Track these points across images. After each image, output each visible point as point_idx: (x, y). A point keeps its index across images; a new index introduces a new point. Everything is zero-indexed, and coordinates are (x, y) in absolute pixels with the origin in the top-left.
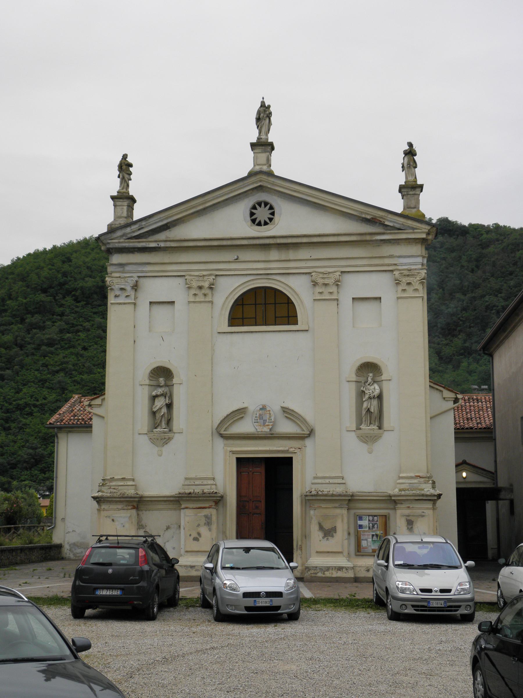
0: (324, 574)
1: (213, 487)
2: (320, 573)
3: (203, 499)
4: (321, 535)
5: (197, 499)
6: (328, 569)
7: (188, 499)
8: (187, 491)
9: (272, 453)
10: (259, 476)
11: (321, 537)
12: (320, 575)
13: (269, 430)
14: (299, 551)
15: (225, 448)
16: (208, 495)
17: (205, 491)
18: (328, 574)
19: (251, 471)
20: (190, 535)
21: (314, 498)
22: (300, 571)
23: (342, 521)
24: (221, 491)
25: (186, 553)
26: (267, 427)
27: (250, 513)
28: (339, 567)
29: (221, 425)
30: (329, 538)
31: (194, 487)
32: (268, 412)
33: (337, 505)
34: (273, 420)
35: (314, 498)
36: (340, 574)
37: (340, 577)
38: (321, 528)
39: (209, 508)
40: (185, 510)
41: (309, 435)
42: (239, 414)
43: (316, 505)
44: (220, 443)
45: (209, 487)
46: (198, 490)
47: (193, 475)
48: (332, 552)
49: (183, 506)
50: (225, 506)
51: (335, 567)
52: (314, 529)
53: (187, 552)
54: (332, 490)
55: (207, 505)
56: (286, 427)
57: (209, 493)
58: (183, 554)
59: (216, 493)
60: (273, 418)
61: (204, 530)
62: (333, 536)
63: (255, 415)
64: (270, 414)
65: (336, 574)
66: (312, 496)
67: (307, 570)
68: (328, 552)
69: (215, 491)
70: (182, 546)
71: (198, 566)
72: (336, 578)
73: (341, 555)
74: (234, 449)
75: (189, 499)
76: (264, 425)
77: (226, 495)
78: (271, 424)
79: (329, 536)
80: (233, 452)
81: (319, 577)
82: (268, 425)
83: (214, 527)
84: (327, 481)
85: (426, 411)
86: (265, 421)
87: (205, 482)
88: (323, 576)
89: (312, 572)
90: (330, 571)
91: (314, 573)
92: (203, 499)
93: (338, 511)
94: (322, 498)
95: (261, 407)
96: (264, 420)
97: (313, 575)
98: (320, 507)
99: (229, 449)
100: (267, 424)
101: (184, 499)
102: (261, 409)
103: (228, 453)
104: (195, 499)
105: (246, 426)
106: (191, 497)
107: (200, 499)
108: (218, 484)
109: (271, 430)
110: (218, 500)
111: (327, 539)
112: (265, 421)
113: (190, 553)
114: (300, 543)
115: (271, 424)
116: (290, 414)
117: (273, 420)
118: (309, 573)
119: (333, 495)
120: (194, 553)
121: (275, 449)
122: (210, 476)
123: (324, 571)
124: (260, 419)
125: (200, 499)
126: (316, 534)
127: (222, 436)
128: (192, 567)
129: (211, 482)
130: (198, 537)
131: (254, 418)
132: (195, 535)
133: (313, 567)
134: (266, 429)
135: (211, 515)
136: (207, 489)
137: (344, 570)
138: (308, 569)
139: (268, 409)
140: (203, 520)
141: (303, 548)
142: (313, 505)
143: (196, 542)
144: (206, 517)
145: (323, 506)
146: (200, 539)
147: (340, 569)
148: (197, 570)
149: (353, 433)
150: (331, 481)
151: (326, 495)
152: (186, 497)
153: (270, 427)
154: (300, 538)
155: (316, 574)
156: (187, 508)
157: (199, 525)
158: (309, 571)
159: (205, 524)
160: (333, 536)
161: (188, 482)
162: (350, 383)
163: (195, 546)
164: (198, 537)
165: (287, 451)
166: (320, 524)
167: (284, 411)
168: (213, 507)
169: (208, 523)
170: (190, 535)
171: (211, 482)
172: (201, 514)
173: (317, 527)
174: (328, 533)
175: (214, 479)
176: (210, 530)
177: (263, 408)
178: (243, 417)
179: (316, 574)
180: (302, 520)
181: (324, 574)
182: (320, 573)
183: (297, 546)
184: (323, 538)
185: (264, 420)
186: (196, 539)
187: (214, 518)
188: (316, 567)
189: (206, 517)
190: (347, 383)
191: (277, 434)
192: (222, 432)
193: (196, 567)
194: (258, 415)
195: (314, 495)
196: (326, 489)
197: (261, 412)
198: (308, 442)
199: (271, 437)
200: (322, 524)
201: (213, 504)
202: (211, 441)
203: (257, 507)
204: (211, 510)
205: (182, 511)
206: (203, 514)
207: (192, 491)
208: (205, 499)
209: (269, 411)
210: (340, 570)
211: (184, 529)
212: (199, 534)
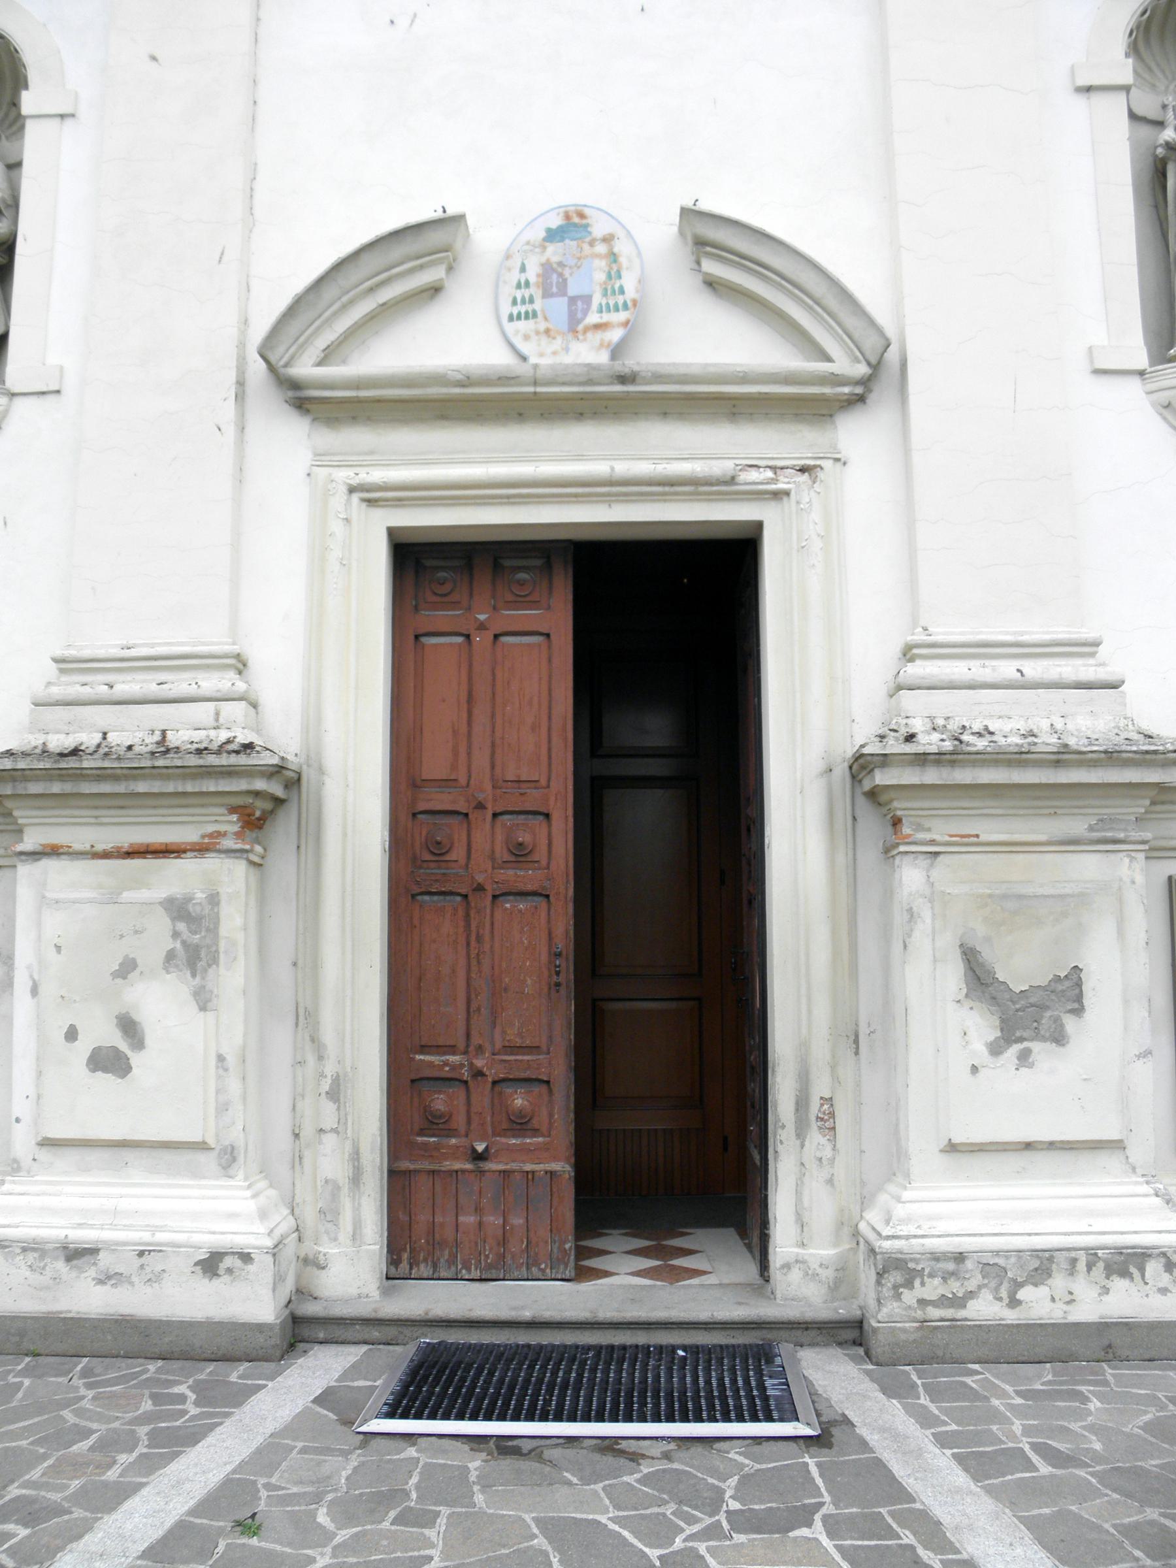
0: (1014, 1303)
1: (235, 711)
2: (986, 1296)
3: (156, 787)
4: (980, 1026)
5: (120, 788)
6: (1042, 1265)
7: (56, 788)
8: (58, 742)
9: (626, 498)
10: (535, 650)
11: (979, 1047)
12: (985, 1309)
13: (603, 358)
14: (816, 1138)
15: (322, 473)
16: (194, 761)
17: (178, 738)
18: (1040, 1304)
19: (482, 627)
20: (72, 1034)
21: (931, 776)
22: (828, 1274)
23: (1121, 933)
24: (283, 738)
25: (44, 1155)
26: (596, 337)
27: (480, 888)
28: (1119, 1250)
29: (295, 327)
30: (1036, 1046)
31: (103, 716)
32: (601, 248)
33: (1077, 826)
34: (631, 293)
35: (931, 776)
36: (1125, 1301)
37: (1127, 1327)
38: (979, 979)
39: (201, 849)
40: (46, 863)
41: (857, 397)
42: (413, 258)
43: (940, 830)
44: (288, 443)
45: (203, 713)
46: (131, 731)
47: (106, 644)
48: (1052, 1146)
49: (30, 841)
50: (310, 838)
51: (1092, 1255)
52: (929, 987)
53: (48, 1143)
54: (1045, 724)
55: (188, 834)
56: (706, 340)
57: (199, 752)
58: (26, 1162)
59: (248, 747)
60: (629, 282)
61: (160, 1001)
62: (1059, 1038)
63: (515, 276)
64: (613, 257)
65: (1094, 1302)
66: (922, 759)
67: (894, 1277)
68: (1028, 1146)
69: (243, 737)
70: (21, 1107)
71: (114, 1247)
72: (1103, 1327)
73: (1112, 1161)
74: (377, 476)
75: (68, 787)
76: (574, 327)
77: (321, 771)
78: (623, 316)
79: (1037, 1036)
80: (372, 496)
81: (983, 1330)
82: (598, 327)
83: (233, 978)
84: (1007, 669)
85: (297, 929)
86: (578, 304)
87: (181, 684)
88: (1011, 1316)
89: (932, 1289)
90: (1059, 1282)
91: (943, 1301)
92: (156, 787)
93: (1088, 867)
94: (987, 776)
95: (556, 221)
96: (573, 300)
97: (934, 1313)
98: (970, 842)
99: (345, 476)
100: (593, 318)
101: (35, 788)
102: (552, 235)
103: (339, 500)
104: (105, 788)
105: (457, 339)
106: (80, 775)
107: (141, 787)
108: (268, 698)
109: (616, 352)
110: (263, 801)
111: (1024, 1058)
112: (578, 304)
113: (72, 1156)
114: (821, 1087)
115: (623, 316)
116: (741, 260)
117: (631, 293)
118: (909, 1297)
119: (1063, 757)
120: (93, 1156)
121: (643, 468)
122: (216, 640)
123: (1017, 1285)
124: (547, 294)
125: (141, 787)
126: (942, 1026)
127: (302, 399)
128: (76, 1254)
129: (223, 682)
130: (123, 1046)
131: (508, 292)
132: (101, 1032)
133: (936, 1257)
134: (588, 354)
135: (214, 899)
136: (188, 727)
137: (1153, 1268)
138: (898, 1269)
139: (598, 230)
140: (160, 933)
141: (842, 1122)
142: (919, 828)
143: (106, 1080)
144: (178, 909)
145: (991, 831)
146: (135, 1059)
147: (1126, 1262)
148: (107, 1278)
149: (1134, 386)
150: (1034, 669)
151: (1019, 758)
152: (48, 775)
153: (615, 335)
154: (820, 1052)
155: (959, 1302)
156: (53, 851)
157: (127, 969)
158: (909, 1284)
159: (170, 956)
160: (1059, 1038)
161: (72, 687)
162: (1098, 99)
163: (102, 1107)
164: (123, 1046)
165: (722, 487)
166: (971, 958)
167: (701, 243)
168: (229, 843)
169: (195, 955)
170: (72, 1034)
171: (223, 682)
172: (144, 895)
173: (953, 977)
174: (1031, 1015)
175: (240, 664)
176: (203, 1001)
177: (572, 225)
178: (435, 291)
179: (959, 1302)
180: (834, 932)
181: (1014, 1303)
182: (986, 1296)
183: (802, 1104)
184: (996, 1050)
185: (573, 300)
186: (109, 1062)
187: (234, 921)
188: (960, 1258)
189: (178, 909)
190: (1081, 101)
191: (659, 378)
192: (305, 368)
193: (104, 1258)
194: (532, 274)
195: (938, 759)
196: (1009, 720)
197: (554, 252)
198: (858, 437)
199: (621, 397)
200: (987, 954)
201: (230, 824)
202: (230, 431)
203: (520, 854)
204: (211, 863)
205: (25, 870)
206: (161, 893)
207: (90, 739)
208: (170, 787)
209: (608, 239)
210: (1124, 1273)
211: (34, 991)
212: (129, 1027)
